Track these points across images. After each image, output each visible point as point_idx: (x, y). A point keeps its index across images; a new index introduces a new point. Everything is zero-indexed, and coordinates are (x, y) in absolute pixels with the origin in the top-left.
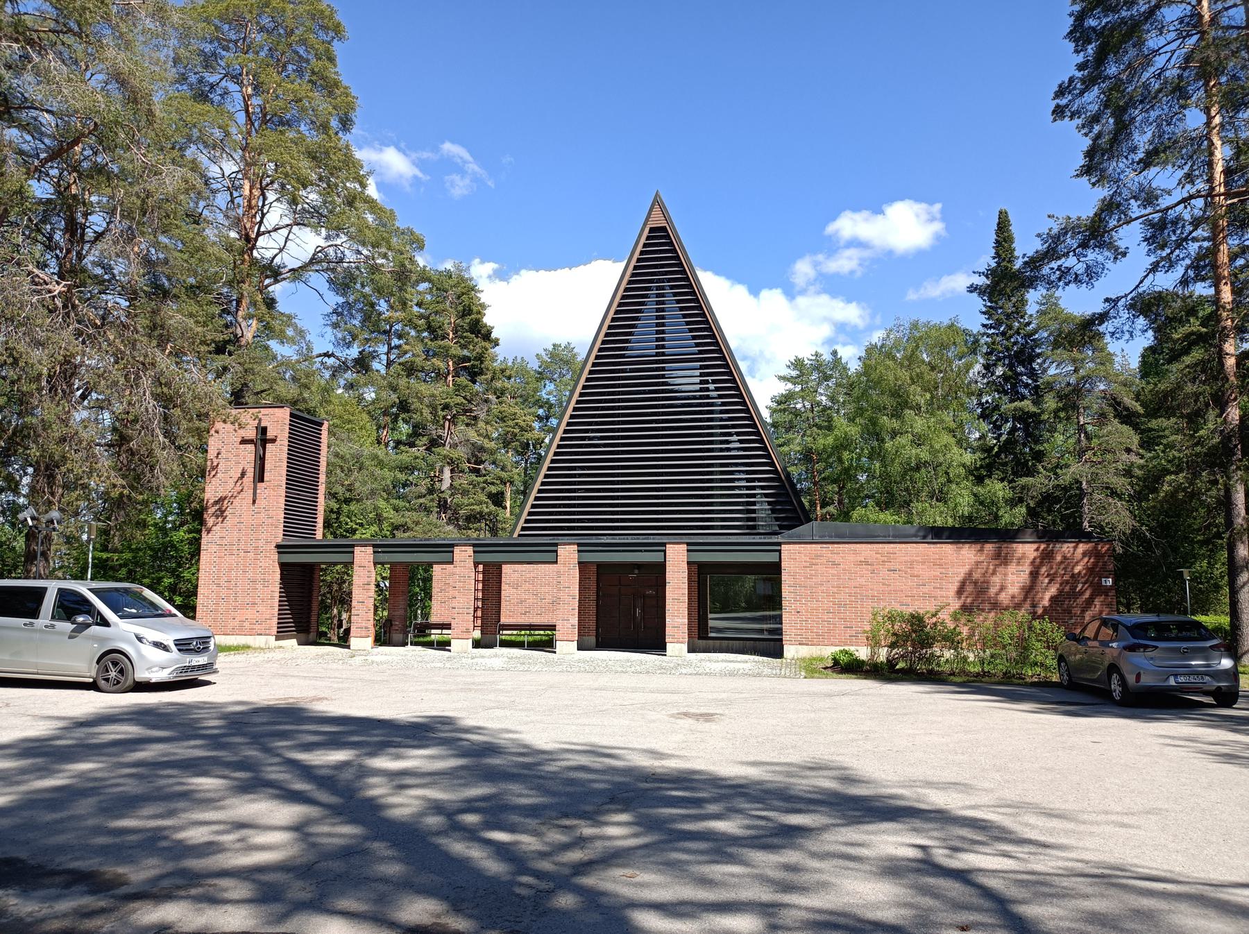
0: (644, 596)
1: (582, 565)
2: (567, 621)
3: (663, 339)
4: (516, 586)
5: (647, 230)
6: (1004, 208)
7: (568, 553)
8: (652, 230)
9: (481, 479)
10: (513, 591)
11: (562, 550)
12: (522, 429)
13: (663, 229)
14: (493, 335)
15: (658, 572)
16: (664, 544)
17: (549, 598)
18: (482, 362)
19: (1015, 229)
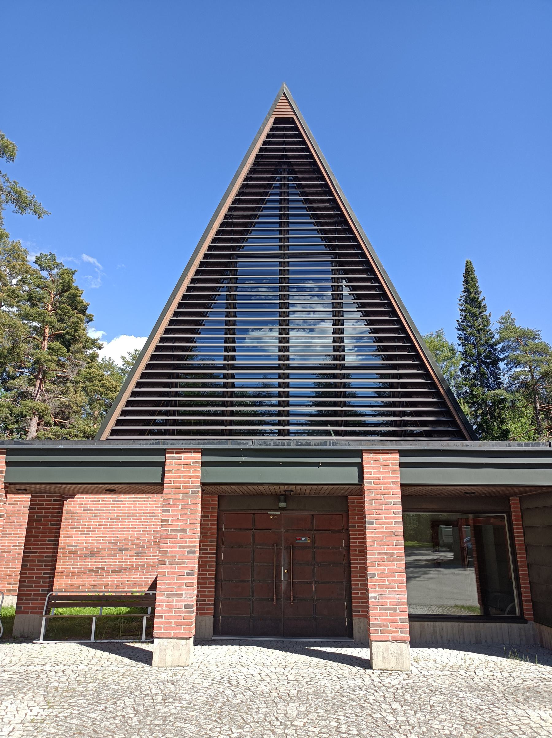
0: (292, 547)
1: (206, 489)
2: (179, 601)
3: (226, 340)
4: (86, 531)
5: (272, 120)
6: (469, 259)
7: (185, 470)
8: (277, 121)
9: (65, 431)
10: (81, 538)
11: (172, 462)
12: (107, 389)
13: (290, 121)
14: (88, 312)
15: (343, 507)
16: (359, 453)
17: (132, 549)
18: (76, 331)
19: (477, 273)
